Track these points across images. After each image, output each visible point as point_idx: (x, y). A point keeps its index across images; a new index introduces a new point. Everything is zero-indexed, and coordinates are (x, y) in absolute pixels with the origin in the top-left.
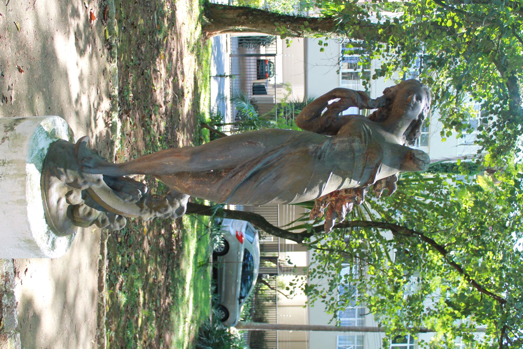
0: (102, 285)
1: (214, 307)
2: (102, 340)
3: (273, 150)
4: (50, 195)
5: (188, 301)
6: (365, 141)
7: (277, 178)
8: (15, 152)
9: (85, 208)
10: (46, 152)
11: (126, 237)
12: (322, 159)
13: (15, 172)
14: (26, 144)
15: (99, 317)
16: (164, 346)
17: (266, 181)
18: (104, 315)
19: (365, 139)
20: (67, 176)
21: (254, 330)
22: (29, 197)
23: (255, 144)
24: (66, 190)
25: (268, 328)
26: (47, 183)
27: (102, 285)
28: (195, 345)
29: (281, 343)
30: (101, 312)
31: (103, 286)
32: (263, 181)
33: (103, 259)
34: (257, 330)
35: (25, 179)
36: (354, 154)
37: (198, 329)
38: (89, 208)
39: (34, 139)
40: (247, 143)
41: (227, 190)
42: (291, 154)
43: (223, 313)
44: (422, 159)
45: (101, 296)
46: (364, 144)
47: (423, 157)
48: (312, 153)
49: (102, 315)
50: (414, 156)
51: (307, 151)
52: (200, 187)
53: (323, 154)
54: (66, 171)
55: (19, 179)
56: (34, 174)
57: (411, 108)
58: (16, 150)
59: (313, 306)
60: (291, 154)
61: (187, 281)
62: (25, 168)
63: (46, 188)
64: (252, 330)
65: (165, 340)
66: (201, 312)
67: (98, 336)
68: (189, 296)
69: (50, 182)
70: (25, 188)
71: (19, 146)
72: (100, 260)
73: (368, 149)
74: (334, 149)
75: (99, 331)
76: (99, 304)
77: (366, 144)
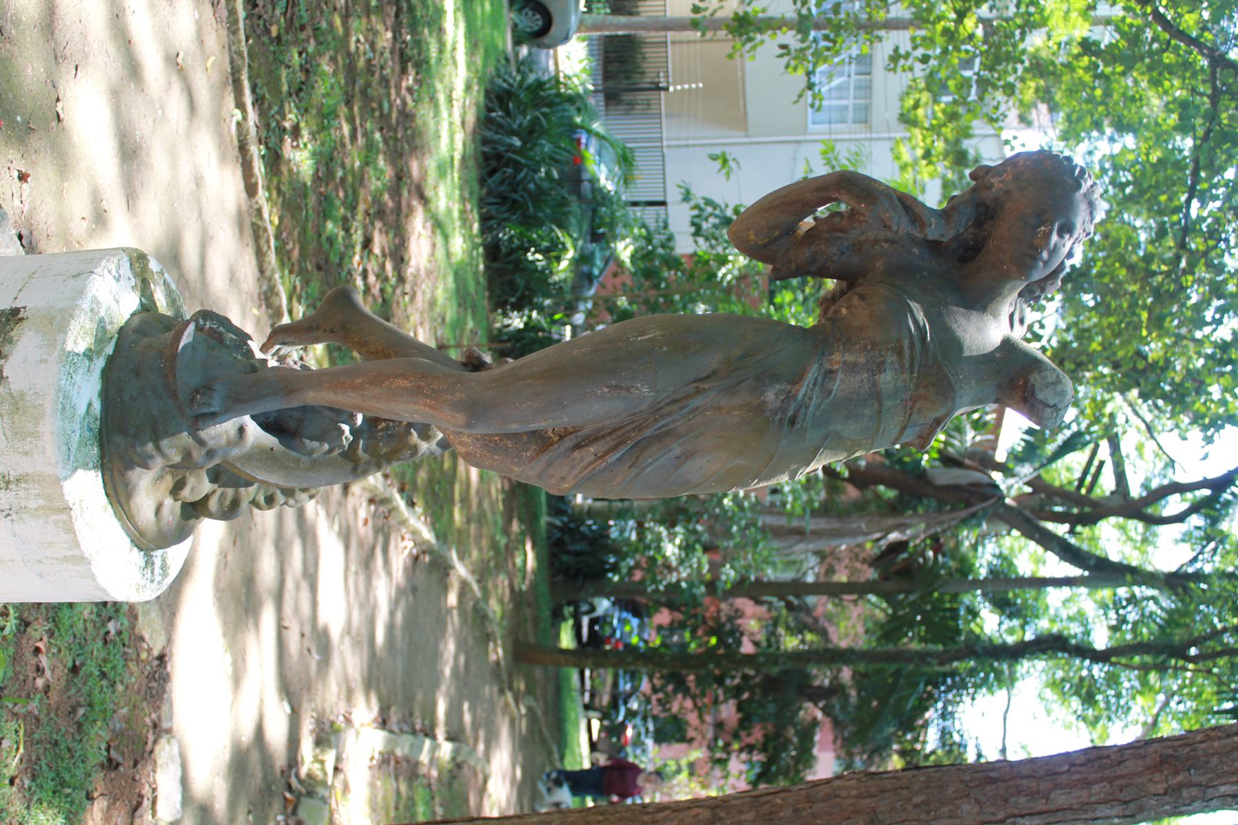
0: (253, 180)
1: (515, 7)
2: (275, 300)
3: (675, 401)
4: (135, 511)
5: (454, 49)
6: (912, 365)
7: (686, 456)
8: (26, 454)
9: (222, 495)
10: (97, 406)
11: (289, 15)
12: (798, 426)
13: (41, 502)
14: (49, 427)
15: (260, 254)
16: (409, 192)
17: (657, 464)
18: (269, 247)
19: (912, 358)
20: (164, 455)
21: (613, 33)
22: (88, 546)
23: (628, 390)
24: (169, 481)
25: (645, 27)
26: (120, 488)
27: (253, 180)
28: (479, 137)
29: (677, 46)
30: (262, 242)
31: (256, 183)
32: (651, 464)
33: (245, 118)
34: (621, 33)
35: (70, 517)
36: (881, 405)
37: (482, 94)
38: (230, 492)
39: (64, 409)
40: (606, 390)
41: (563, 478)
42: (719, 408)
43: (538, 16)
44: (1052, 402)
45: (256, 207)
46: (906, 376)
47: (1055, 394)
48: (775, 412)
49: (265, 249)
50: (1033, 394)
51: (760, 408)
52: (494, 460)
53: (803, 411)
54: (158, 448)
55: (55, 517)
56: (86, 487)
57: (1041, 264)
58: (27, 448)
59: (754, 57)
60: (719, 408)
61: (446, 8)
62: (62, 495)
63: (122, 499)
64: (607, 33)
65: (410, 177)
66: (486, 51)
67: (265, 293)
68: (454, 43)
69: (127, 485)
70: (75, 535)
71: (31, 434)
72: (238, 124)
73: (917, 386)
74: (830, 392)
75: (266, 282)
76: (253, 224)
77: (912, 372)
